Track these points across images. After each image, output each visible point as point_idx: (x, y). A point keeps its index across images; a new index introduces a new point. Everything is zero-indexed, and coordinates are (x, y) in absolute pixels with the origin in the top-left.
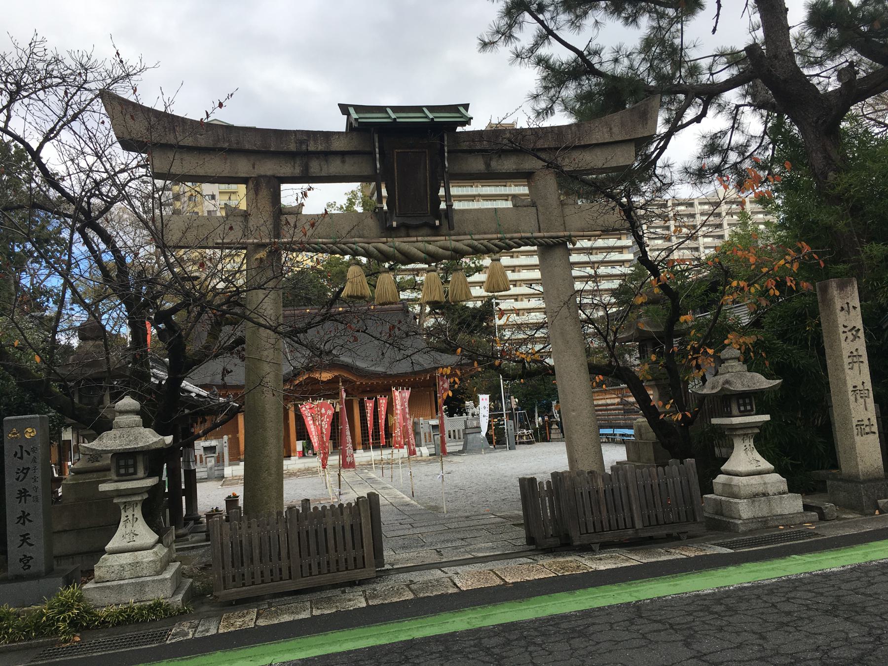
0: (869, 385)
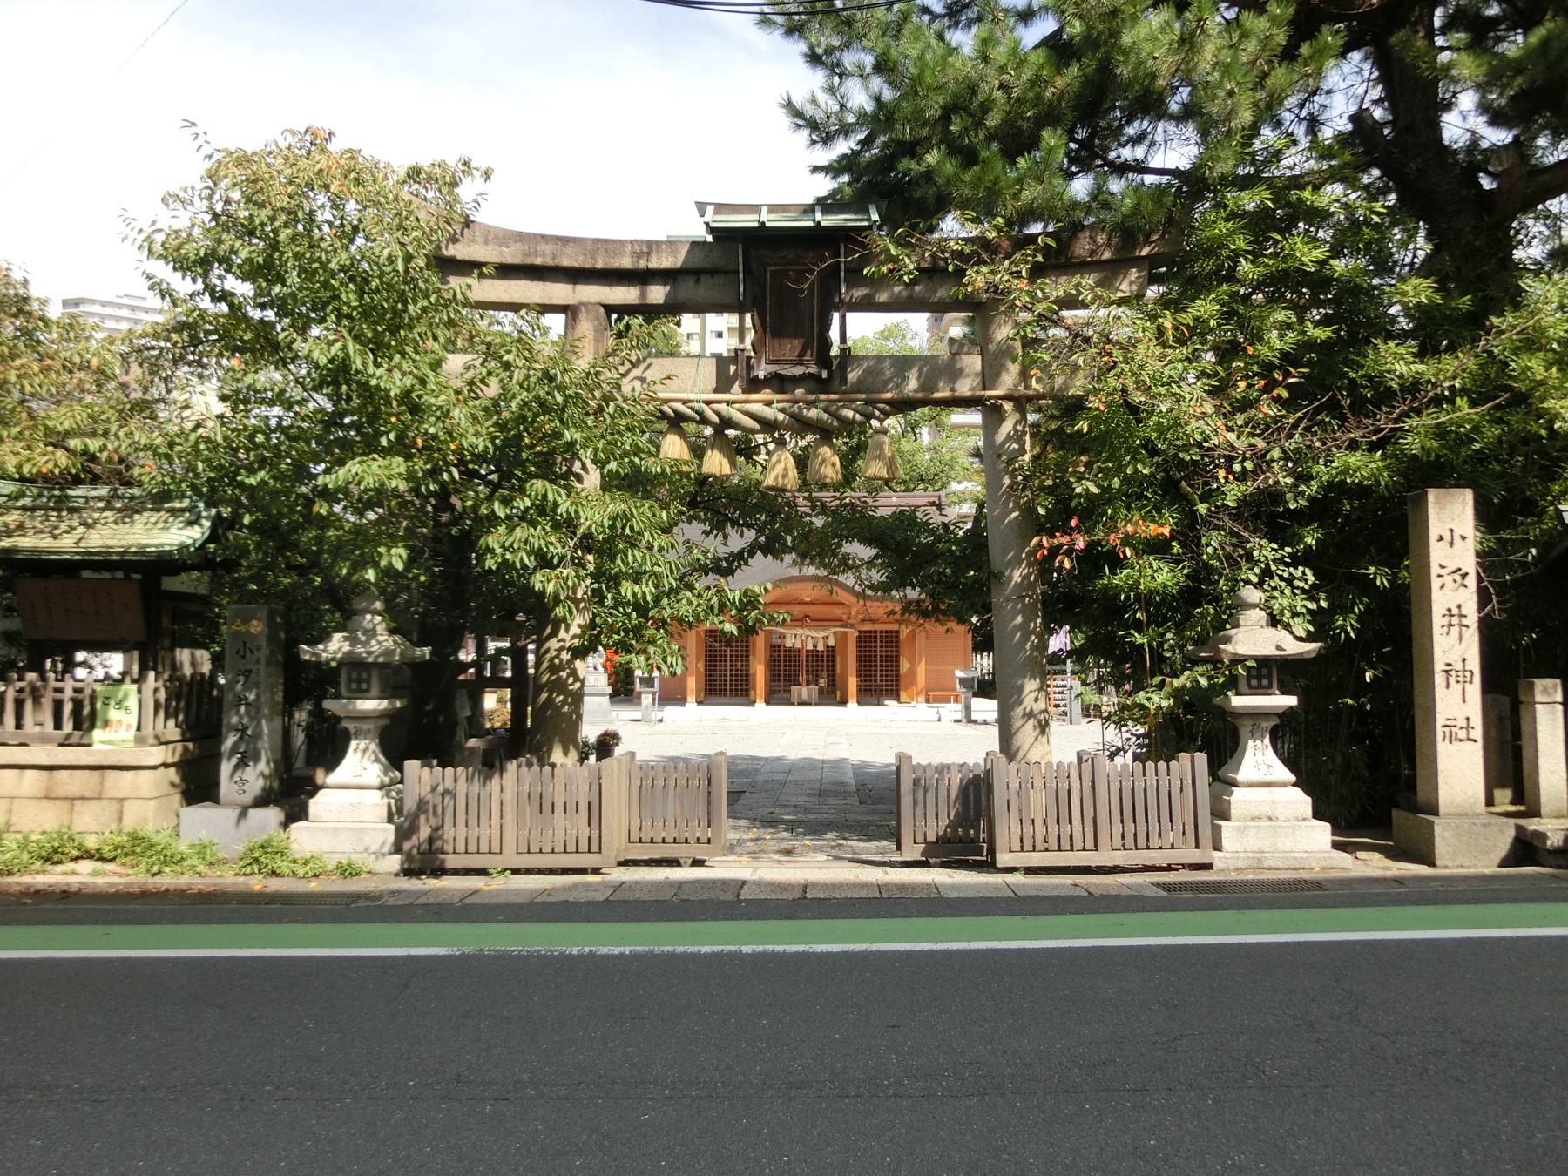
0: (1474, 664)
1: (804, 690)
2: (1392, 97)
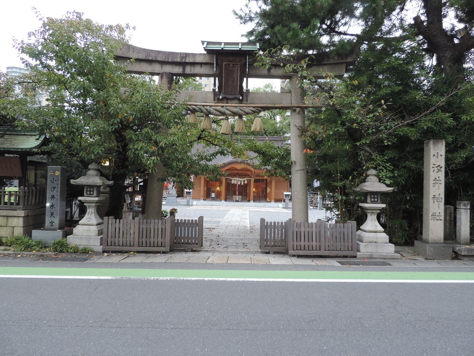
0: (443, 196)
1: (237, 197)
2: (428, 13)
